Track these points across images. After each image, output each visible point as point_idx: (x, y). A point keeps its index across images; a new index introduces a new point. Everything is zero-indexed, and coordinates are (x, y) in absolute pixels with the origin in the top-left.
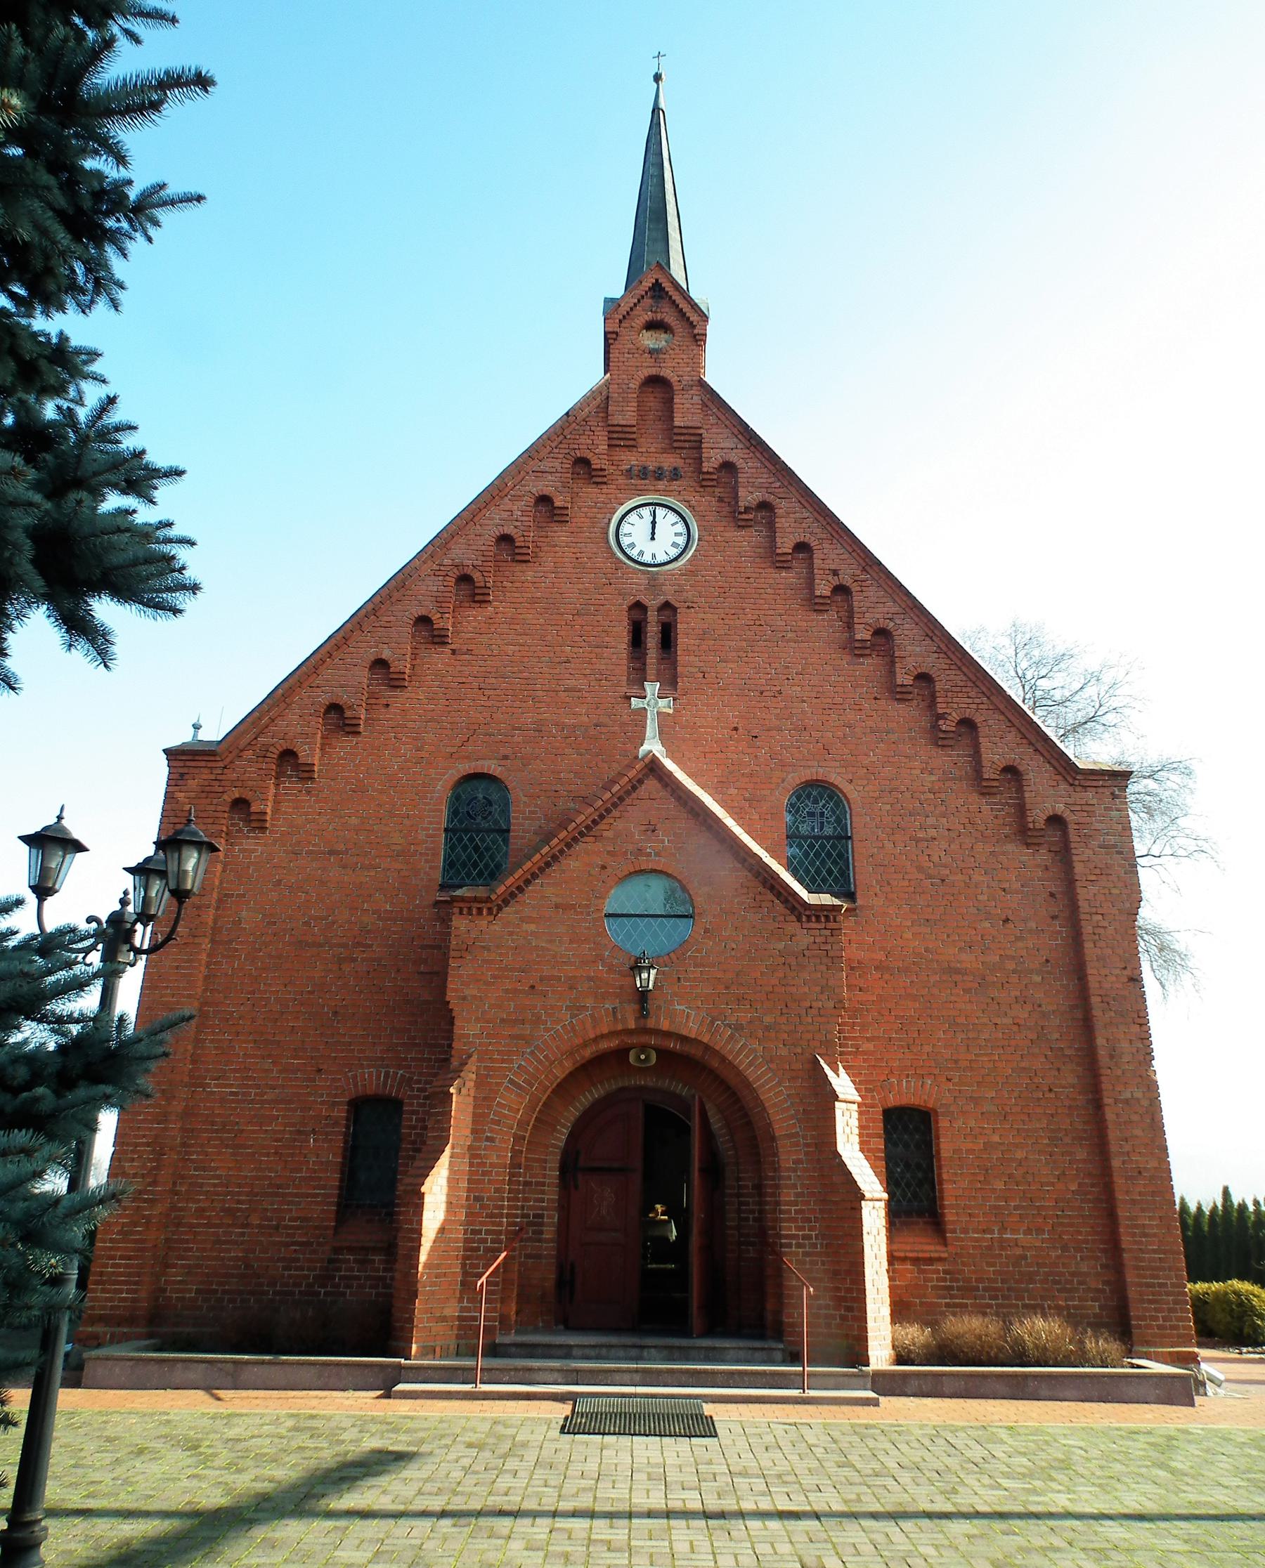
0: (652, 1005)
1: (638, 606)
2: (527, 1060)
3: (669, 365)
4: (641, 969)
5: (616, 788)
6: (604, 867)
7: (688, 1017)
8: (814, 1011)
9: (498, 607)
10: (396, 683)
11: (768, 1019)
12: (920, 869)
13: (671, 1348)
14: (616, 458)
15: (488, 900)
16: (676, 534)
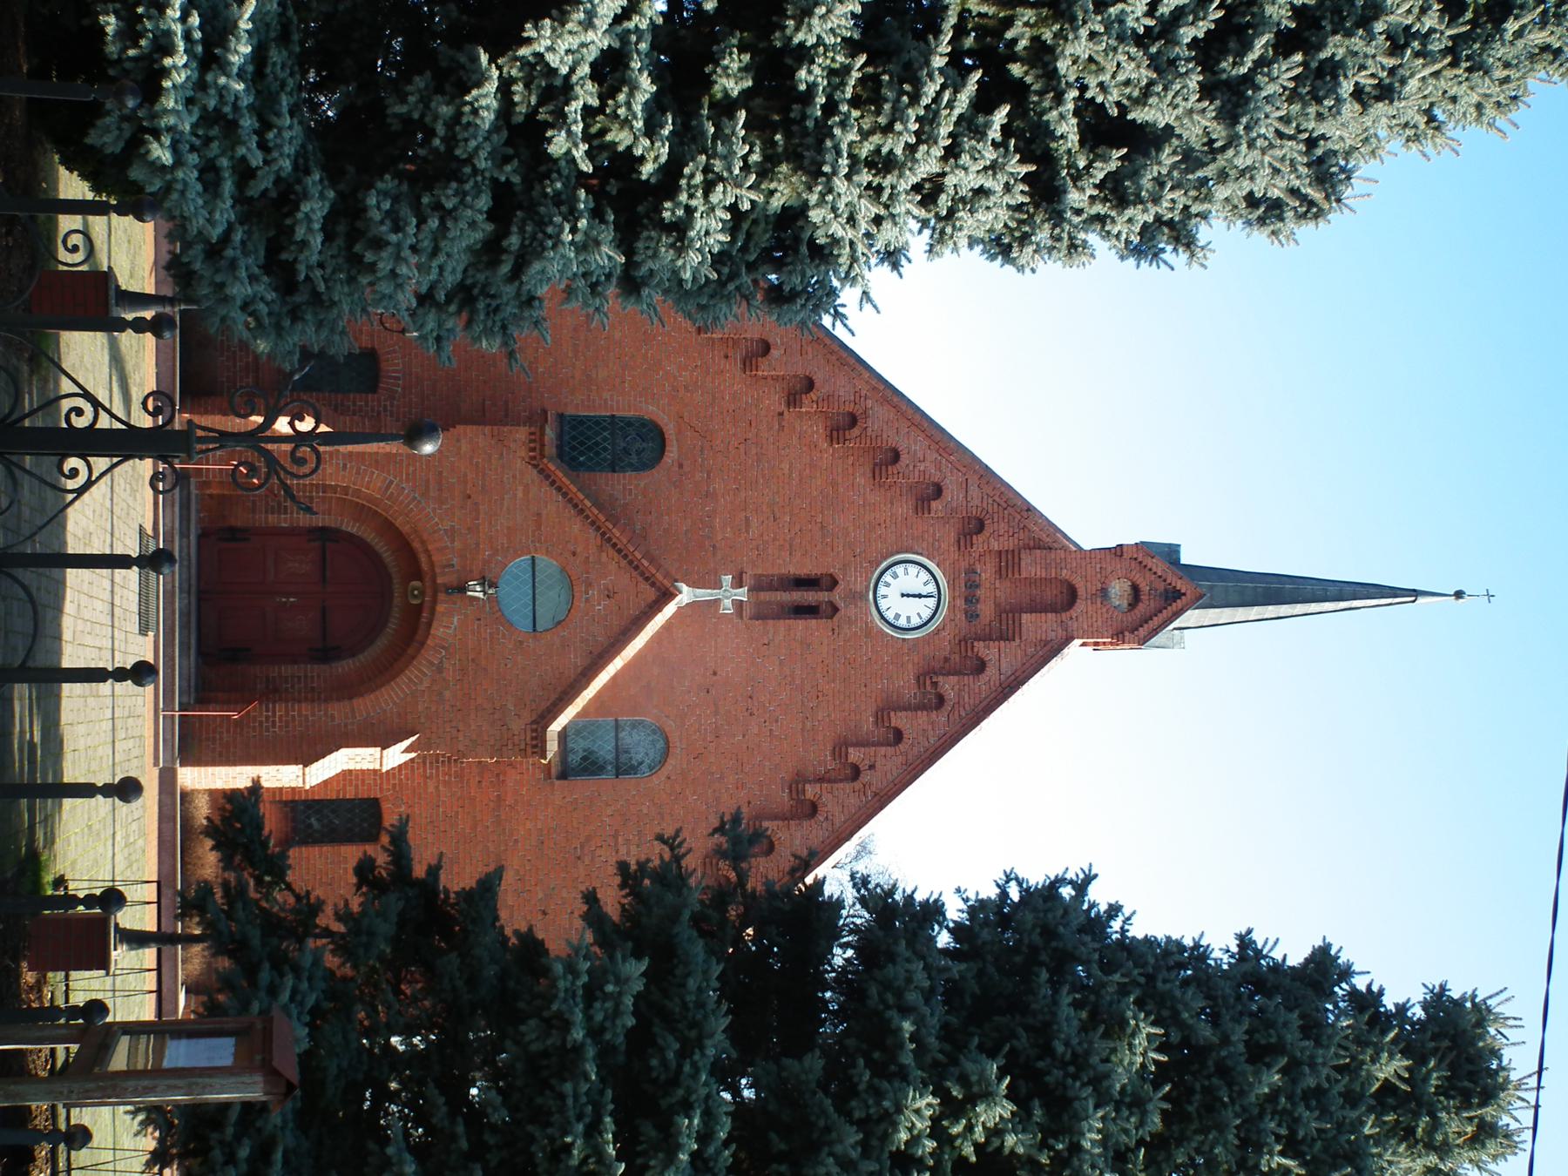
0: (457, 597)
1: (833, 583)
2: (408, 495)
3: (1090, 609)
4: (482, 584)
5: (646, 563)
6: (574, 554)
7: (449, 628)
8: (454, 732)
9: (827, 453)
10: (749, 362)
11: (447, 694)
12: (589, 839)
13: (189, 613)
14: (988, 559)
15: (543, 456)
16: (908, 618)
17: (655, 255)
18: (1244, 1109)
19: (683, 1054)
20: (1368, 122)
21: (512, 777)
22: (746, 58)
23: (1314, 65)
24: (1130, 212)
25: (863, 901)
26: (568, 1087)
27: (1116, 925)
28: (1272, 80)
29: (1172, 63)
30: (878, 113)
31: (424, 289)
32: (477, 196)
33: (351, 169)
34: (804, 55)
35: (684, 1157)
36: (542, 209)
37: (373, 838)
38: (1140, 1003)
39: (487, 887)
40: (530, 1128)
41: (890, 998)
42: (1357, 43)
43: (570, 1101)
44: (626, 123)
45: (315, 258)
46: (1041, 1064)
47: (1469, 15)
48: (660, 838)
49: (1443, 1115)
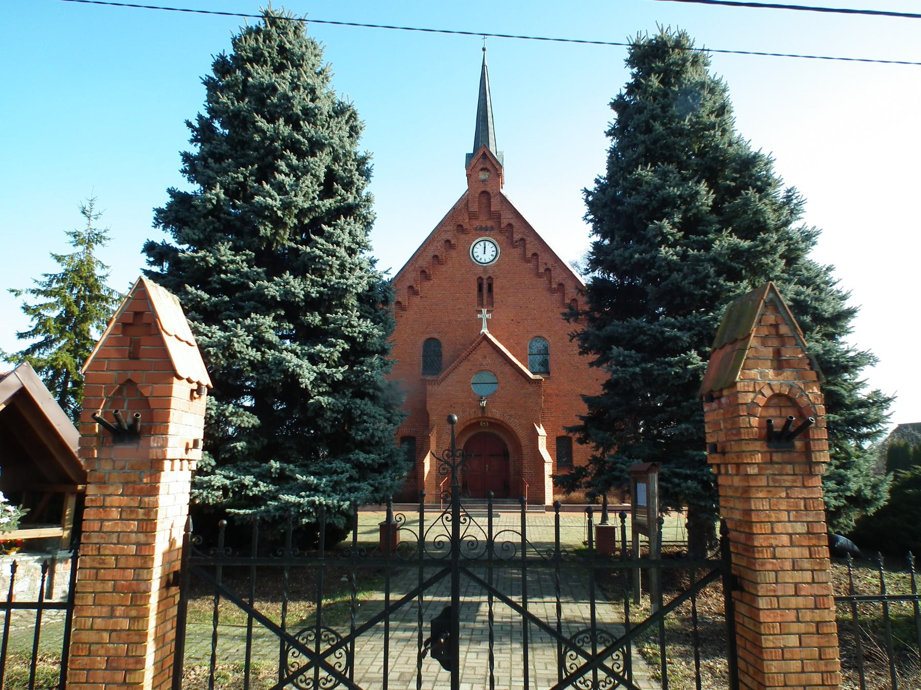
1: (480, 278)
11: (520, 413)
12: (571, 364)
17: (374, 344)
18: (668, 135)
19: (645, 334)
20: (322, 97)
21: (549, 391)
22: (308, 314)
23: (304, 117)
24: (355, 180)
25: (593, 271)
26: (656, 373)
27: (602, 181)
28: (309, 131)
29: (305, 167)
30: (325, 270)
31: (386, 421)
32: (356, 403)
33: (348, 444)
34: (307, 294)
35: (679, 334)
36: (360, 382)
37: (570, 438)
38: (630, 173)
39: (588, 400)
40: (669, 385)
41: (627, 262)
42: (295, 102)
43: (660, 372)
44: (332, 354)
45: (377, 457)
46: (651, 209)
47: (285, 61)
48: (571, 341)
49: (671, 61)
